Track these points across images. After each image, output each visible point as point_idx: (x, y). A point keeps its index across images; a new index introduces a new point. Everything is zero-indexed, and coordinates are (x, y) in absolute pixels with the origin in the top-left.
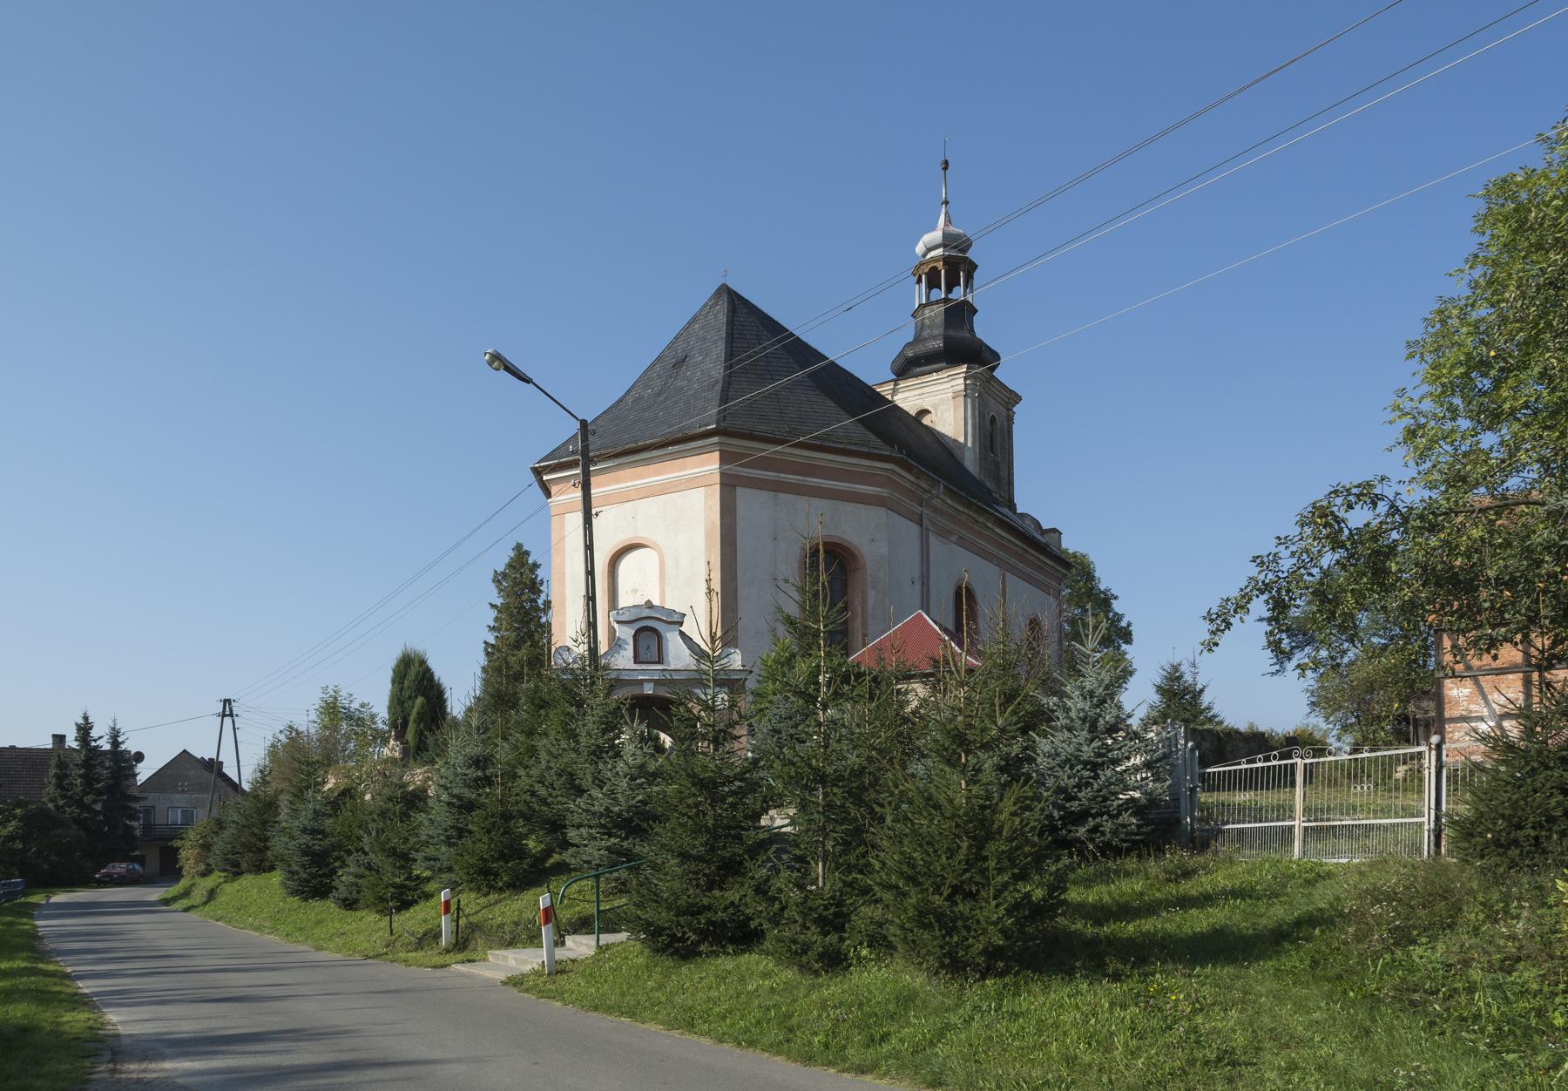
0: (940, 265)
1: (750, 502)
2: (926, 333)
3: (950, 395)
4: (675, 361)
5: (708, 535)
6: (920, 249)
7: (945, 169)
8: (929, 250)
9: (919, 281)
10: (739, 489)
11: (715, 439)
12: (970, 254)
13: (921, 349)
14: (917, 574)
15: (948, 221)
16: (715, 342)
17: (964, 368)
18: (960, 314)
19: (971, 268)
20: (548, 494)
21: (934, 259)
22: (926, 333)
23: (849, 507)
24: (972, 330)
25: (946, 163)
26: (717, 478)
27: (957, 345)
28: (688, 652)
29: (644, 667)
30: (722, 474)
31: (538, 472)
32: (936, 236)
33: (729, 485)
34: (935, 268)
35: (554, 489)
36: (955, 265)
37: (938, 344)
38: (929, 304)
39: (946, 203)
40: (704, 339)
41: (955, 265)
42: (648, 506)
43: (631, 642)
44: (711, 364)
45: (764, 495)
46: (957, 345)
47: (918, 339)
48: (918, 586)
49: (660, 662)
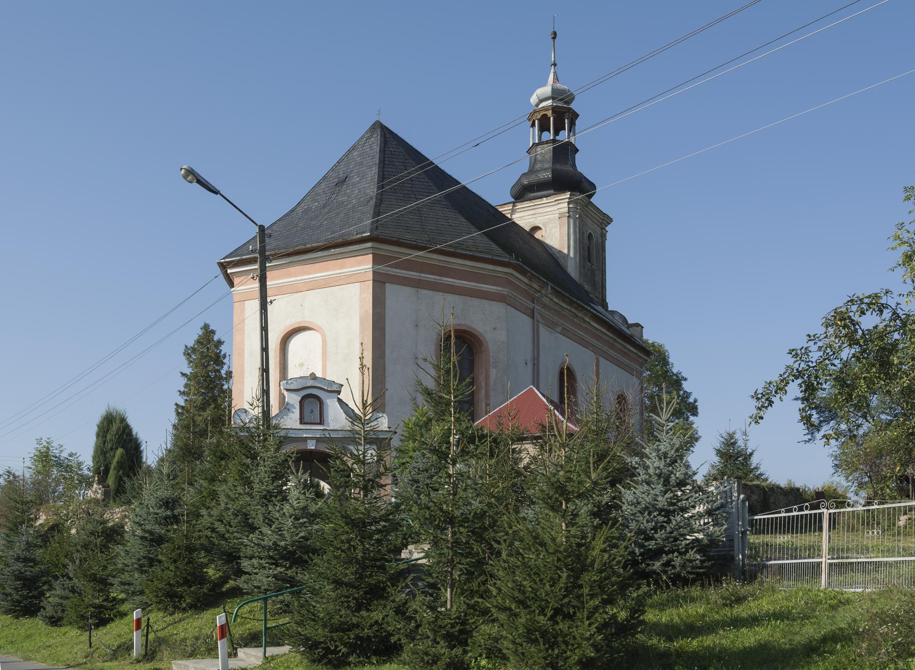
0: (549, 113)
1: (395, 294)
2: (538, 166)
3: (557, 216)
4: (338, 180)
5: (362, 321)
6: (534, 100)
7: (554, 38)
8: (541, 101)
9: (533, 125)
10: (387, 285)
11: (369, 245)
12: (573, 106)
13: (533, 178)
14: (529, 357)
15: (556, 79)
16: (370, 167)
17: (568, 195)
18: (565, 152)
19: (574, 116)
20: (231, 284)
21: (545, 109)
22: (538, 166)
23: (476, 302)
24: (574, 166)
25: (555, 33)
26: (370, 276)
27: (563, 177)
28: (344, 415)
29: (308, 427)
30: (374, 272)
31: (223, 266)
32: (547, 90)
33: (380, 282)
34: (545, 115)
35: (236, 281)
36: (561, 114)
37: (548, 175)
38: (541, 143)
39: (555, 65)
40: (361, 164)
41: (561, 114)
42: (314, 297)
43: (298, 407)
44: (366, 184)
45: (408, 290)
46: (563, 177)
47: (532, 171)
48: (530, 365)
49: (321, 422)
